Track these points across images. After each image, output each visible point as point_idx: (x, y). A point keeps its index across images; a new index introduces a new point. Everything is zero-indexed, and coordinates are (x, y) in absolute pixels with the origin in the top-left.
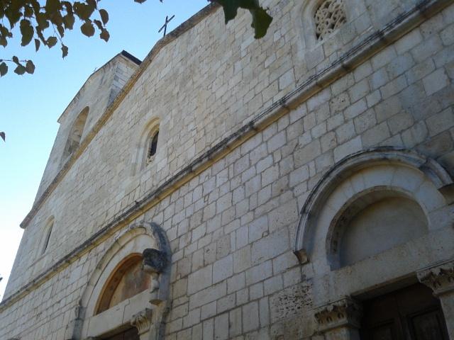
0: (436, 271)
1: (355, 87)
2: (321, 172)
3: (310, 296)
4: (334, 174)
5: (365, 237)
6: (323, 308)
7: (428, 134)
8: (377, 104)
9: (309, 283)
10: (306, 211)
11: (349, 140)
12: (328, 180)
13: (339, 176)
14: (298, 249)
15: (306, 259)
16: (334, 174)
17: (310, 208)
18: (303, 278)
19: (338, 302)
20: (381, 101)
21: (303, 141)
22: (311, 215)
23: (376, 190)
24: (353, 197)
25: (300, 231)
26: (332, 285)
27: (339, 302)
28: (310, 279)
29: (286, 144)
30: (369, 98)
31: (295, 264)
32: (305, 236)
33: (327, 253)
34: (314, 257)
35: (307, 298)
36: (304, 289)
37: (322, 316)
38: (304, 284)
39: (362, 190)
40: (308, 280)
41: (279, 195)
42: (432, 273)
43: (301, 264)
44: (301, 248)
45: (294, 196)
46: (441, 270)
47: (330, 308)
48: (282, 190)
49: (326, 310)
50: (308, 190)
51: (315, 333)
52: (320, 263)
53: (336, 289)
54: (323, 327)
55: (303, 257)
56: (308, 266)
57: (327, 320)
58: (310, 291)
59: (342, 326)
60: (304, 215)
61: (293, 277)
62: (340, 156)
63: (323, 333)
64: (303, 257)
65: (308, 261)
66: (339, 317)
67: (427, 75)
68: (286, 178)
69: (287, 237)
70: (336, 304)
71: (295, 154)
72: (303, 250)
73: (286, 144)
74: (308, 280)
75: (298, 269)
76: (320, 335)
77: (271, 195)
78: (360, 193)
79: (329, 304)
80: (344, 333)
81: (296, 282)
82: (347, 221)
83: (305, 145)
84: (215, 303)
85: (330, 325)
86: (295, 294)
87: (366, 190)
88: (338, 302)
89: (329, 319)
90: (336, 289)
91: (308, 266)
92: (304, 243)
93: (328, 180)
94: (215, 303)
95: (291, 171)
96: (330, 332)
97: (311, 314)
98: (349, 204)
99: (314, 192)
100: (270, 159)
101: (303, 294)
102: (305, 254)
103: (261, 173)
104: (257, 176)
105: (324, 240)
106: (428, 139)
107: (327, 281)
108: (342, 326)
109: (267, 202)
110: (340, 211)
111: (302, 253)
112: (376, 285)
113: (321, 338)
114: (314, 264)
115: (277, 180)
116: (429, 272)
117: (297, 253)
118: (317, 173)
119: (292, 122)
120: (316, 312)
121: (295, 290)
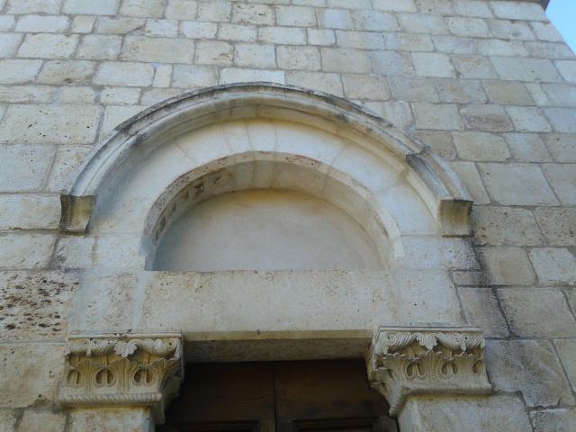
0: (428, 341)
1: (287, 8)
2: (185, 89)
3: (60, 309)
4: (225, 97)
5: (224, 236)
6: (103, 344)
7: (413, 123)
8: (327, 47)
9: (68, 279)
10: (132, 131)
11: (258, 68)
12: (208, 102)
13: (233, 105)
14: (79, 193)
15: (83, 224)
16: (225, 97)
17: (144, 128)
18: (55, 262)
19: (154, 339)
20: (334, 46)
21: (153, 27)
22: (144, 140)
23: (297, 162)
24: (245, 155)
25: (98, 163)
26: (138, 299)
27: (159, 342)
28: (78, 270)
29: (112, 17)
30: (312, 32)
31: (44, 224)
32: (108, 175)
33: (145, 231)
34: (105, 227)
35: (47, 310)
36: (48, 288)
37: (90, 363)
38: (53, 276)
39: (268, 150)
40: (67, 270)
41: (58, 86)
42: (415, 342)
43: (64, 230)
44: (90, 192)
45: (97, 100)
46: (438, 341)
47: (126, 349)
48: (69, 81)
49: (110, 352)
50: (139, 103)
51: (40, 404)
52: (120, 244)
53: (147, 311)
54: (69, 393)
55: (74, 214)
56: (84, 243)
57: (98, 378)
58: (64, 296)
59: (134, 405)
60: (124, 137)
61: (36, 251)
62: (228, 77)
63: (66, 408)
64: (74, 214)
65: (86, 232)
66: (137, 377)
67: (420, 52)
68: (91, 65)
69: (44, 165)
70: (148, 344)
71: (129, 40)
72: (91, 199)
73: (112, 17)
74: (67, 270)
75: (50, 239)
76: (55, 412)
77: (36, 77)
78: (262, 152)
79: (125, 339)
80: (139, 420)
81: (30, 264)
82: (201, 195)
83: (156, 37)
84: (38, 64)
85: (104, 391)
86: (13, 291)
87: (276, 154)
88: (154, 339)
89: (105, 375)
90: (147, 311)
91: (80, 240)
92: (102, 185)
93: (208, 102)
94: (38, 64)
95: (107, 60)
96: (89, 412)
97: (51, 356)
98: (229, 163)
99: (168, 107)
100: (63, 22)
101: (39, 298)
102: (89, 213)
103: (25, 34)
104: (9, 37)
105: (149, 204)
106: (413, 128)
107: (124, 287)
108: (134, 405)
109: (19, 84)
110: (206, 166)
111: (81, 207)
112: (259, 333)
113: (56, 422)
114: (101, 242)
115: (63, 59)
116: (410, 337)
117: (68, 202)
118: (171, 87)
119: (21, 53)
120: (77, 347)
121: (17, 282)
